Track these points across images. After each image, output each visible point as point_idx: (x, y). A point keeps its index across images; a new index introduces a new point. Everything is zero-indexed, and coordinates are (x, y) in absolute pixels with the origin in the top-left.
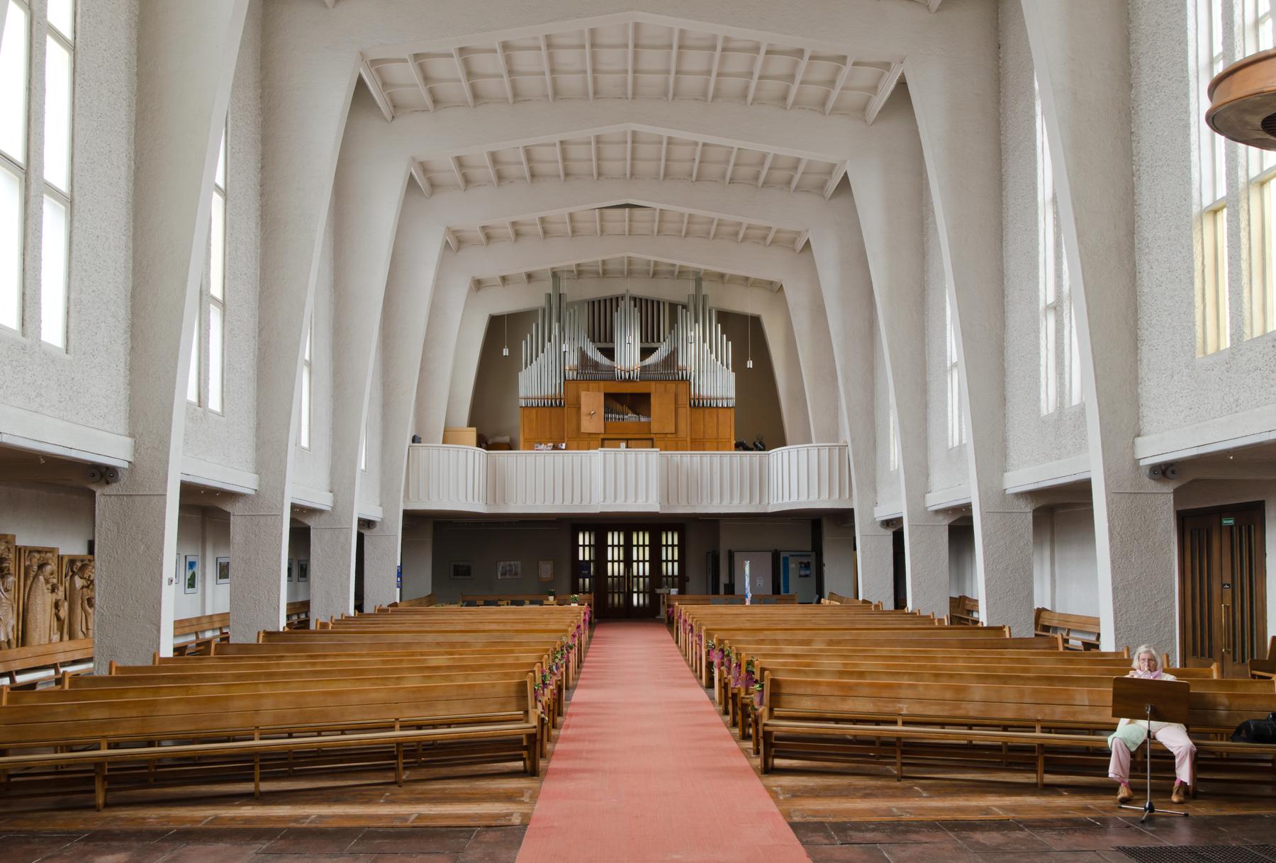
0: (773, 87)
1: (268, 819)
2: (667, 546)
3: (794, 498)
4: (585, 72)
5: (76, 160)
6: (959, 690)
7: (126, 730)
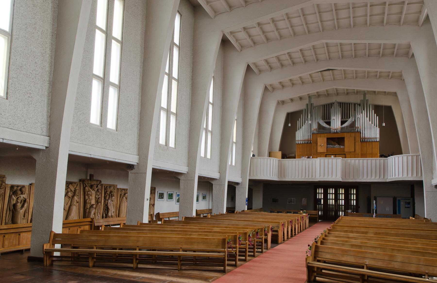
0: (377, 18)
1: (123, 276)
2: (330, 194)
3: (397, 176)
4: (303, 25)
5: (121, 75)
6: (391, 256)
7: (101, 244)
